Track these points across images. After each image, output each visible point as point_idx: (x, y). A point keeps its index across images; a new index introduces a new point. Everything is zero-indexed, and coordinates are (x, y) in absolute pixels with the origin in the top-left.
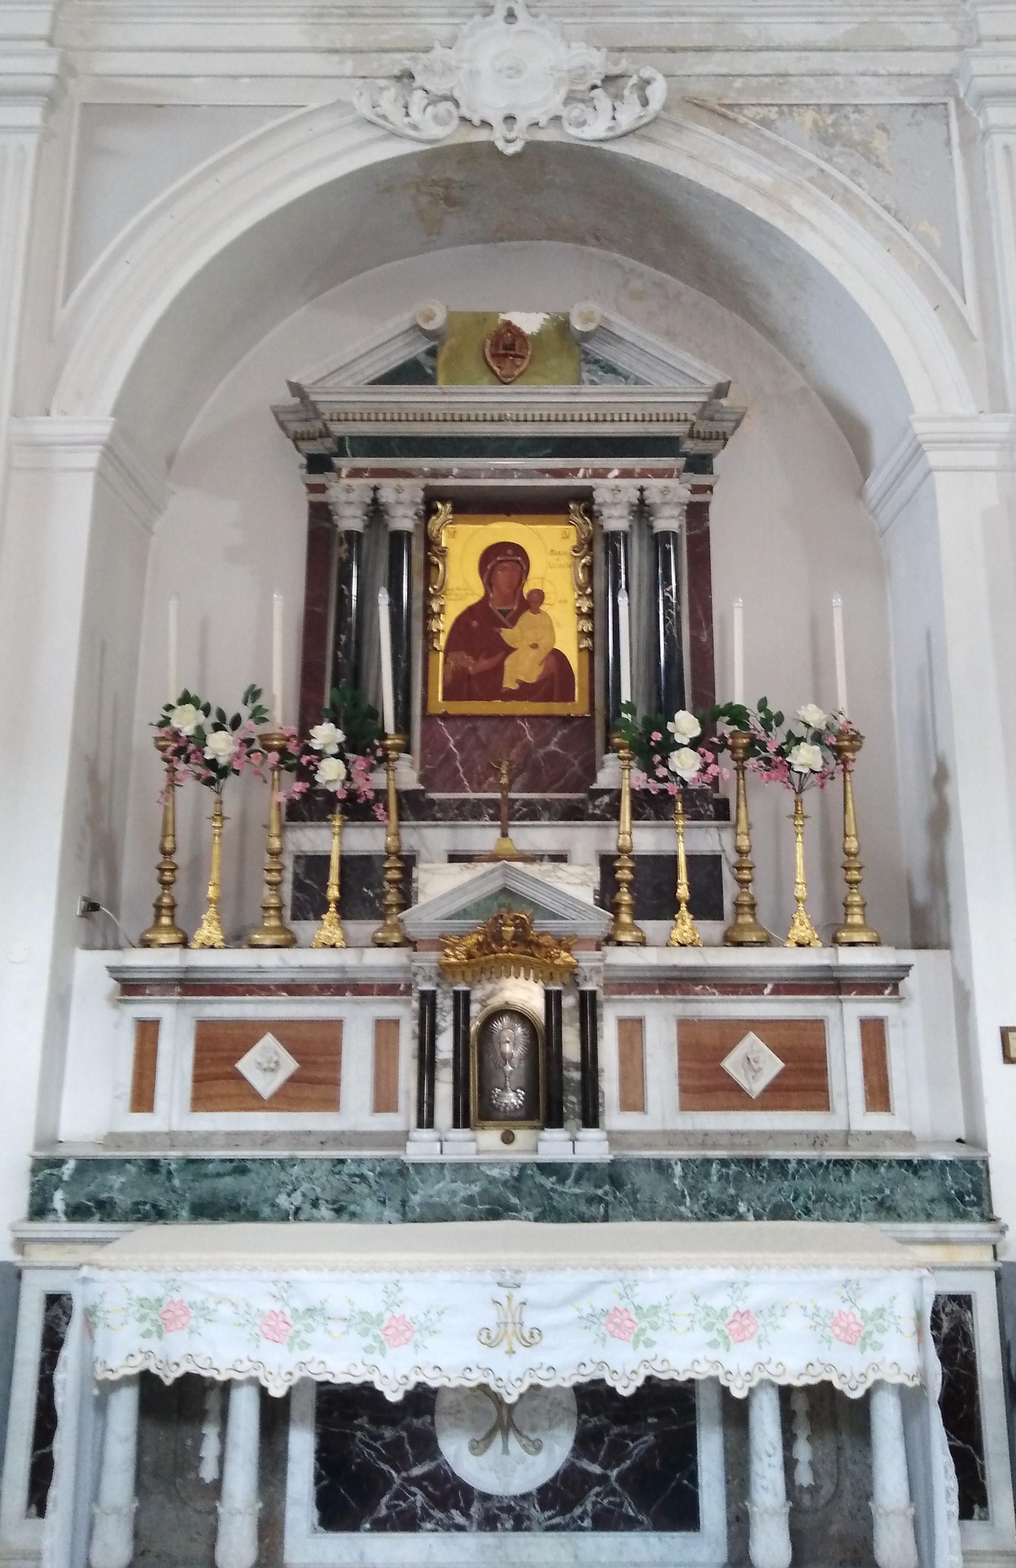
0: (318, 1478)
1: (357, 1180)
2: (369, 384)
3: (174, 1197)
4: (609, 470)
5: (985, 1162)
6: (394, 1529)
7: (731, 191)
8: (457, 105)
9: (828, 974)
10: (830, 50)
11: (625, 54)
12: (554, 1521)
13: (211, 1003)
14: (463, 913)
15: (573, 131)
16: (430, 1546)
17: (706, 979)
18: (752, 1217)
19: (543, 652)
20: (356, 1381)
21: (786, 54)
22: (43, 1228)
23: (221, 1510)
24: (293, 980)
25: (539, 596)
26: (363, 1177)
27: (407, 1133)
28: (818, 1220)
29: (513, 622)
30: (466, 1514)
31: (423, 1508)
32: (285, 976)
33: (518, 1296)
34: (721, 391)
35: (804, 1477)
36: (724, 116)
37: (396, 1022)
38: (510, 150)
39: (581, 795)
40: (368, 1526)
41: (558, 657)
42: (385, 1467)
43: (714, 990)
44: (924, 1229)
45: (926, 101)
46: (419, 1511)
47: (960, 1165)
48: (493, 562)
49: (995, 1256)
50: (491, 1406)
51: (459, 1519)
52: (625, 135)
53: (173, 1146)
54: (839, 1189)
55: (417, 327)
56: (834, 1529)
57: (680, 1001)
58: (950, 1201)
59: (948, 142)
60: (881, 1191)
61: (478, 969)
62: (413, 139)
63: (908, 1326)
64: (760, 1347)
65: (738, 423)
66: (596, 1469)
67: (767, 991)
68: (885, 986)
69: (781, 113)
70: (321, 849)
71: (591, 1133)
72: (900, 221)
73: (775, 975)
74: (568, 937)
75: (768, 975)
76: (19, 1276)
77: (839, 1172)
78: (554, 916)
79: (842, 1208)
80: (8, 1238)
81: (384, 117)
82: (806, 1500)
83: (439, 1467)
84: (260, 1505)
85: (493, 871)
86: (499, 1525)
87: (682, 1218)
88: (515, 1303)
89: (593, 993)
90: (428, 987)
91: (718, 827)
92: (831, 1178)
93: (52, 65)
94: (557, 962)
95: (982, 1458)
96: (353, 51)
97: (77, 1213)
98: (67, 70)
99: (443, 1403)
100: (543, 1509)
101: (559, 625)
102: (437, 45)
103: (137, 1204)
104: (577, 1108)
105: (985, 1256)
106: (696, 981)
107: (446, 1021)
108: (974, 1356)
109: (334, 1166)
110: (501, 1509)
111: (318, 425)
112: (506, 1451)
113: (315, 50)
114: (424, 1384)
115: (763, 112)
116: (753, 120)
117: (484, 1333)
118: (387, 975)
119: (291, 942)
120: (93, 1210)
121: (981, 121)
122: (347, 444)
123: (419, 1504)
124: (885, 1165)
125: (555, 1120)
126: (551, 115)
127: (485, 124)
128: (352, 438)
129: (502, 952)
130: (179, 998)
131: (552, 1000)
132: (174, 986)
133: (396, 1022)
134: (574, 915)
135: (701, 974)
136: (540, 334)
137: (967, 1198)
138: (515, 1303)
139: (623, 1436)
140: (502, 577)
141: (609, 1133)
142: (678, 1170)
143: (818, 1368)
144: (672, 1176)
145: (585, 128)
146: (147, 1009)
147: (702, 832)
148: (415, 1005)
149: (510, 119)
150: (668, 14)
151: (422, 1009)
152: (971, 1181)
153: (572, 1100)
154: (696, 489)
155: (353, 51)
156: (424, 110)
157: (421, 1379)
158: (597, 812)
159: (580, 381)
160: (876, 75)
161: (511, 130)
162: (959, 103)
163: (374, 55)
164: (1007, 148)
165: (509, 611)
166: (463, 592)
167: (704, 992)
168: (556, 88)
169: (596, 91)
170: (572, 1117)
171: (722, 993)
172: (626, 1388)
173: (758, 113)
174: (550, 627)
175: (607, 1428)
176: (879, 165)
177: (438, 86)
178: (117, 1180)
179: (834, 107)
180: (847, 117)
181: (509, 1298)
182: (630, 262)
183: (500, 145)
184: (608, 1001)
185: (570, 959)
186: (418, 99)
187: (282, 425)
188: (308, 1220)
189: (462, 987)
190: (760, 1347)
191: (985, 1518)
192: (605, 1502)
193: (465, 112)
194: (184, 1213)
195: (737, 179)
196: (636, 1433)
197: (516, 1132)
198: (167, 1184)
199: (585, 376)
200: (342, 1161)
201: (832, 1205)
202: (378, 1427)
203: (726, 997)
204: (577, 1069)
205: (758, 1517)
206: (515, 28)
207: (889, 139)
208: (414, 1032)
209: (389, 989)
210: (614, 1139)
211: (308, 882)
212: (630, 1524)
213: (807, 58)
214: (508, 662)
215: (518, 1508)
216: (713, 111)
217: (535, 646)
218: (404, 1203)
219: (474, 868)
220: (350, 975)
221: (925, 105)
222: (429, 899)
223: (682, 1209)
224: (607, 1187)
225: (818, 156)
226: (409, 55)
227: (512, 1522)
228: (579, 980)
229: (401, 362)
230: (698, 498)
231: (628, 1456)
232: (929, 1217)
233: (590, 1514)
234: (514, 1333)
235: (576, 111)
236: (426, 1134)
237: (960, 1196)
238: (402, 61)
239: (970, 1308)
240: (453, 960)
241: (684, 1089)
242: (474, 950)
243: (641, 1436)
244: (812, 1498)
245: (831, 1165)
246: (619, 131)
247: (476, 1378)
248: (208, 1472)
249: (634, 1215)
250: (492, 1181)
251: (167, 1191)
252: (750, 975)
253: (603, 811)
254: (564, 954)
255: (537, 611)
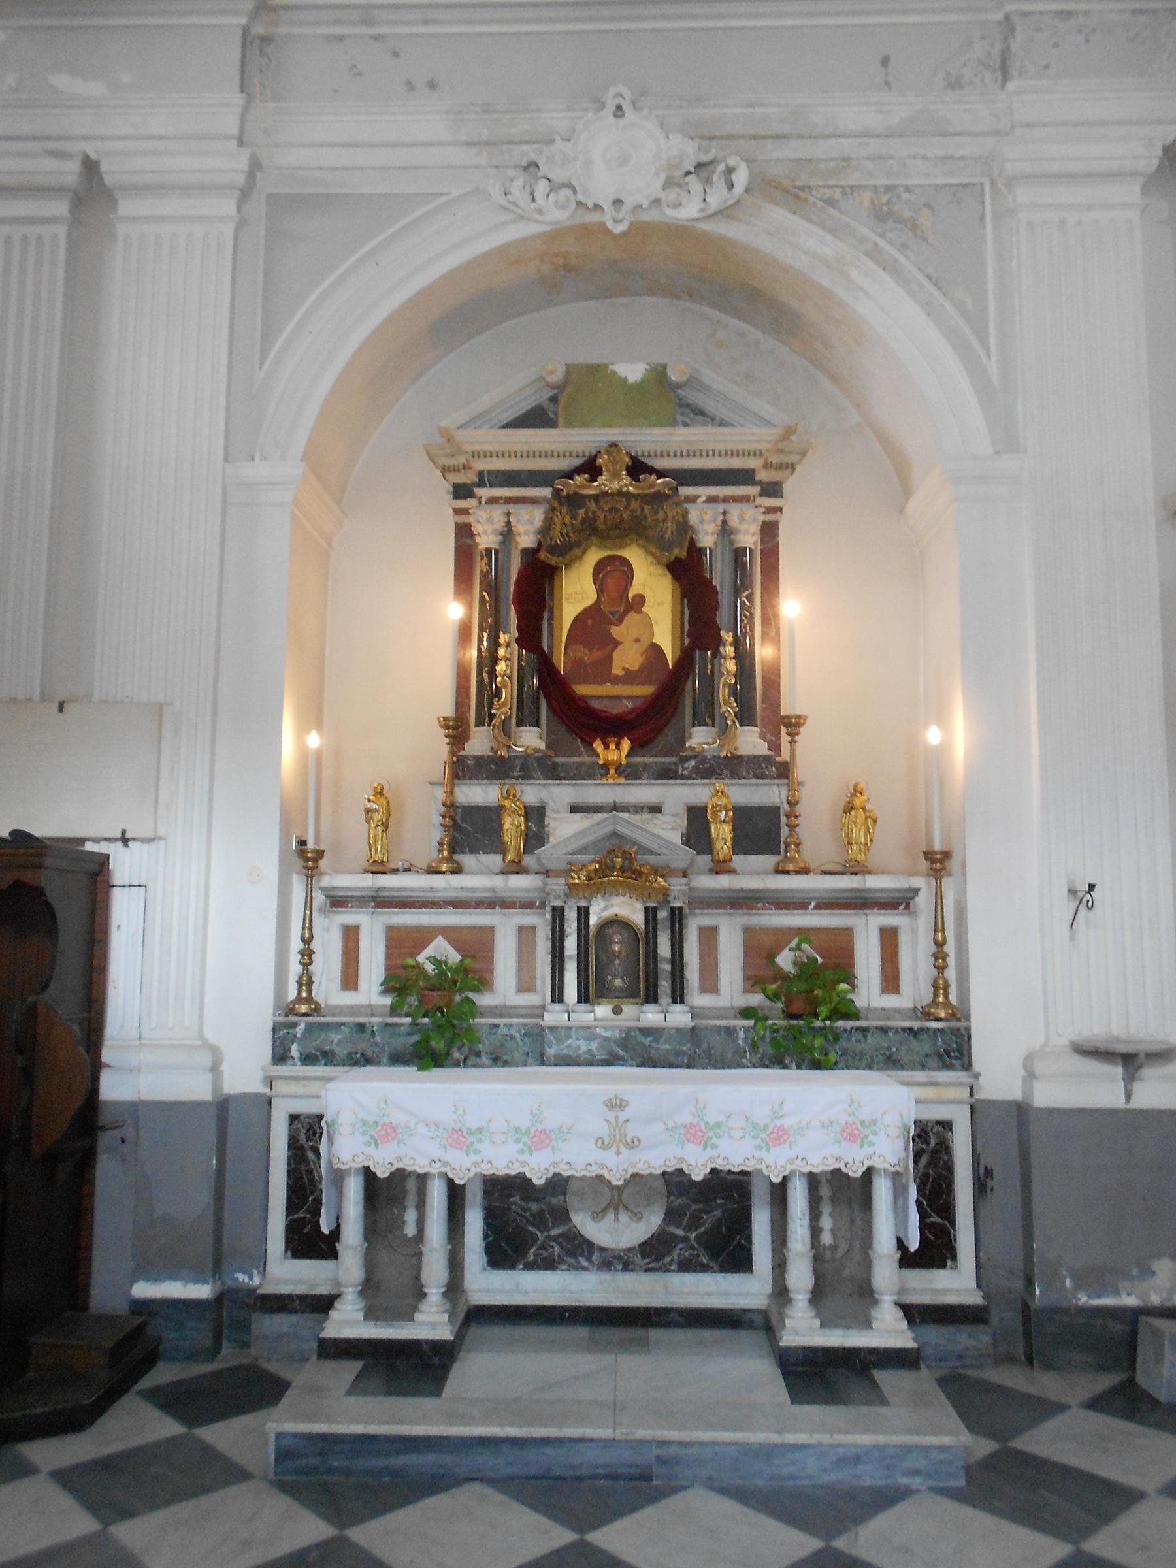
0: (486, 1236)
1: (508, 1039)
2: (504, 427)
3: (377, 1049)
4: (698, 497)
5: (968, 1030)
6: (539, 1268)
7: (801, 263)
8: (575, 191)
9: (858, 894)
10: (887, 136)
11: (714, 143)
12: (652, 1265)
13: (397, 913)
14: (583, 850)
15: (669, 212)
16: (565, 1280)
17: (765, 898)
18: (794, 1065)
19: (645, 645)
20: (513, 1173)
21: (850, 140)
22: (284, 1070)
23: (423, 1249)
24: (457, 897)
25: (641, 599)
26: (512, 1037)
27: (543, 1007)
28: (843, 1069)
29: (620, 621)
30: (589, 1260)
31: (559, 1255)
32: (451, 895)
33: (623, 1116)
34: (789, 432)
35: (826, 1239)
36: (797, 196)
37: (534, 928)
38: (619, 229)
39: (673, 759)
40: (521, 1267)
41: (656, 649)
42: (532, 1229)
43: (772, 907)
44: (920, 1076)
45: (966, 181)
46: (556, 1258)
47: (949, 1031)
48: (604, 572)
49: (972, 1094)
50: (607, 1190)
51: (585, 1263)
52: (715, 214)
53: (372, 1015)
54: (859, 1048)
55: (541, 378)
56: (846, 1273)
57: (746, 914)
58: (940, 1056)
59: (982, 218)
60: (889, 1048)
61: (595, 889)
62: (536, 221)
63: (894, 1132)
64: (791, 1149)
65: (804, 454)
66: (680, 1232)
67: (811, 907)
68: (899, 904)
69: (844, 193)
70: (473, 800)
71: (678, 1008)
72: (939, 288)
73: (817, 895)
74: (662, 868)
75: (811, 895)
76: (270, 1103)
77: (859, 1036)
78: (651, 853)
79: (860, 1060)
80: (259, 1075)
81: (515, 204)
82: (828, 1255)
83: (570, 1230)
84: (449, 1247)
85: (605, 820)
86: (613, 1268)
87: (743, 1066)
88: (621, 1121)
89: (680, 909)
90: (558, 903)
91: (778, 785)
92: (853, 1039)
93: (243, 163)
94: (655, 885)
95: (954, 1229)
96: (487, 143)
97: (308, 1059)
98: (255, 166)
99: (573, 1187)
100: (643, 1257)
101: (656, 623)
102: (558, 139)
103: (351, 1053)
104: (669, 991)
105: (966, 1093)
106: (758, 900)
107: (571, 927)
108: (953, 1162)
109: (492, 1029)
110: (614, 1257)
111: (462, 460)
112: (617, 1219)
113: (455, 144)
114: (559, 1174)
115: (828, 192)
116: (820, 200)
117: (600, 1142)
118: (526, 895)
119: (457, 870)
120: (320, 1058)
121: (1010, 197)
122: (486, 476)
123: (556, 1253)
124: (893, 1031)
125: (652, 997)
126: (653, 197)
127: (597, 207)
128: (489, 472)
129: (613, 876)
130: (373, 910)
131: (650, 914)
132: (369, 901)
133: (534, 928)
134: (667, 852)
135: (762, 895)
136: (642, 382)
137: (952, 1054)
138: (621, 1121)
139: (700, 1211)
140: (611, 583)
141: (692, 1008)
142: (742, 1034)
143: (831, 1161)
144: (737, 1037)
145: (682, 210)
146: (350, 917)
147: (766, 788)
148: (549, 916)
149: (618, 202)
150: (752, 106)
151: (554, 920)
152: (956, 1042)
153: (665, 986)
154: (770, 510)
155: (487, 143)
156: (548, 196)
157: (557, 1171)
158: (685, 772)
159: (674, 423)
160: (924, 158)
161: (618, 211)
162: (993, 183)
163: (504, 147)
164: (1030, 224)
165: (617, 612)
166: (580, 596)
167: (764, 908)
168: (657, 174)
169: (690, 177)
170: (664, 996)
171: (777, 909)
172: (698, 1175)
173: (825, 194)
174: (649, 625)
175: (688, 1206)
176: (924, 239)
177: (558, 175)
178: (336, 1037)
179: (888, 189)
180: (899, 197)
181: (617, 1118)
182: (716, 314)
183: (610, 224)
184: (691, 914)
185: (663, 883)
186: (542, 187)
187: (432, 459)
188: (474, 1066)
189: (583, 903)
190: (791, 1149)
191: (955, 1268)
192: (687, 1254)
193: (580, 197)
194: (385, 1060)
195: (806, 253)
196: (708, 1209)
197: (624, 1007)
198: (372, 1040)
199: (679, 417)
200: (496, 1026)
201: (853, 1058)
202: (527, 1204)
203: (781, 911)
204: (668, 963)
205: (791, 1258)
206: (622, 122)
207: (934, 215)
208: (547, 936)
209: (528, 905)
210: (695, 1013)
211: (464, 825)
212: (704, 1268)
213: (867, 144)
214: (615, 654)
215: (625, 1257)
216: (788, 192)
217: (637, 640)
218: (542, 1054)
219: (592, 817)
220: (498, 895)
221: (965, 185)
222: (558, 840)
223: (744, 1060)
224: (689, 1045)
225: (873, 231)
226: (534, 146)
227: (621, 1265)
228: (670, 899)
229: (529, 408)
230: (770, 517)
231: (703, 1224)
232: (923, 1067)
233: (676, 1261)
234: (621, 1140)
235: (672, 195)
236: (557, 1007)
237: (947, 1053)
238: (530, 153)
239: (951, 1130)
240: (577, 881)
241: (747, 978)
242: (593, 875)
243: (712, 1211)
244: (832, 1253)
245: (853, 1031)
246: (709, 212)
247: (592, 1172)
248: (410, 1230)
249: (709, 1064)
250: (606, 1039)
251: (371, 1045)
252: (798, 895)
253: (690, 772)
254: (660, 879)
255: (639, 612)
